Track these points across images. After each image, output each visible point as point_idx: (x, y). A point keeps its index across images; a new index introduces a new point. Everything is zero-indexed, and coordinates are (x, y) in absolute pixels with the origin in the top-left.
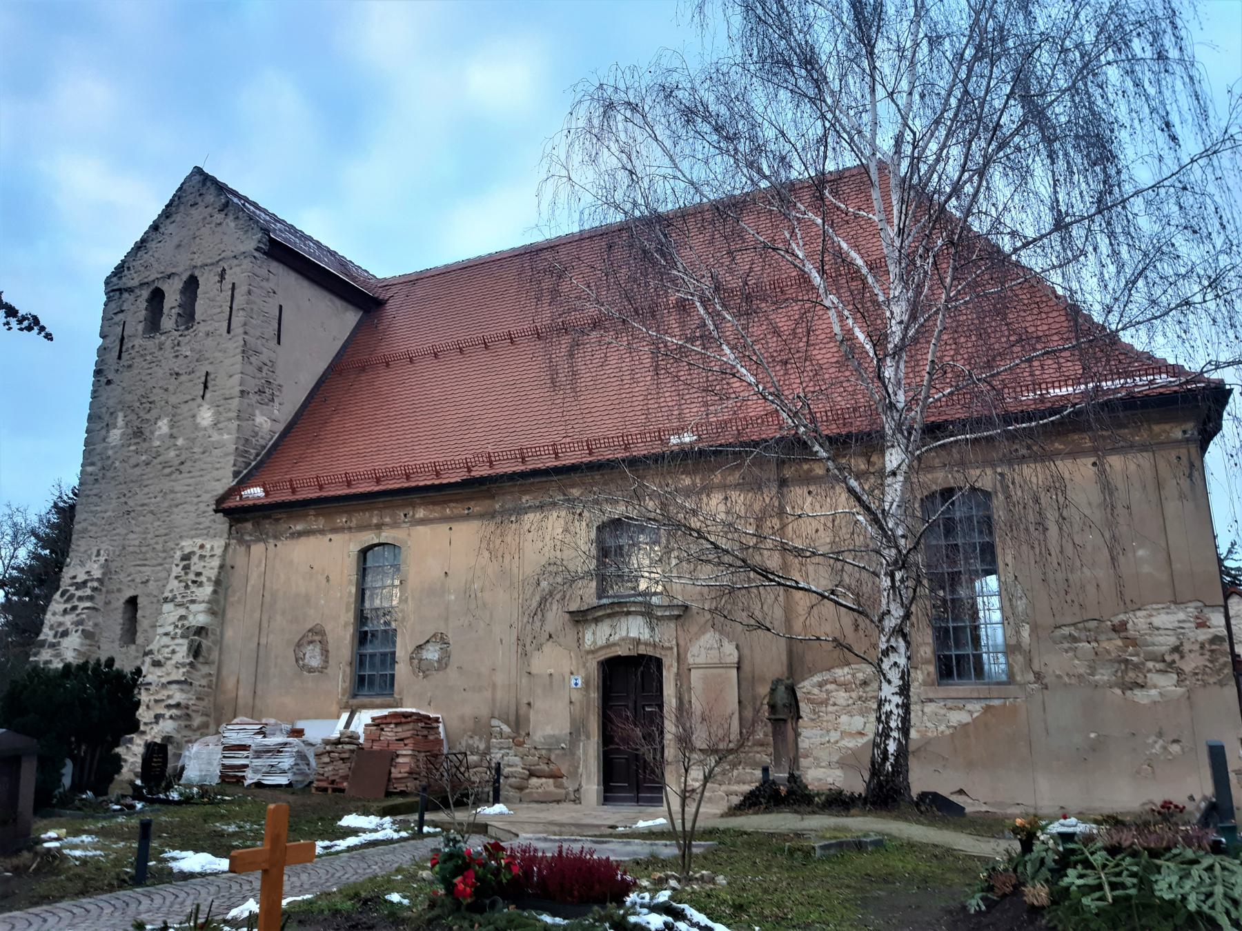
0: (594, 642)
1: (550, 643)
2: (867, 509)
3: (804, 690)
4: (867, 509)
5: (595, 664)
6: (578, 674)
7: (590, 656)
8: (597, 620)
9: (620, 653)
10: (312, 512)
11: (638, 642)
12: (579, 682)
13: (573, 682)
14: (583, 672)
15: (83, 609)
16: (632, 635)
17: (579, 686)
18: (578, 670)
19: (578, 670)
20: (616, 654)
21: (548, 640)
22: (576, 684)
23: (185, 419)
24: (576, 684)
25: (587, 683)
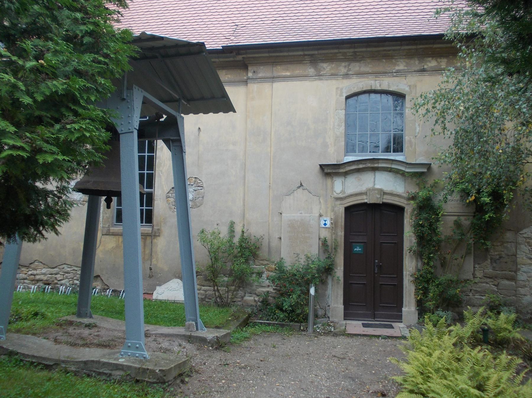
0: (343, 192)
1: (300, 190)
2: (413, 72)
3: (525, 235)
4: (413, 72)
5: (342, 210)
6: (326, 216)
7: (338, 202)
8: (346, 174)
9: (366, 201)
10: (384, 61)
11: (383, 193)
12: (328, 223)
13: (322, 223)
14: (331, 215)
15: (87, 21)
16: (377, 186)
17: (328, 226)
18: (326, 212)
19: (326, 212)
20: (362, 201)
21: (299, 187)
22: (325, 224)
23: (511, 380)
24: (325, 224)
25: (335, 224)
